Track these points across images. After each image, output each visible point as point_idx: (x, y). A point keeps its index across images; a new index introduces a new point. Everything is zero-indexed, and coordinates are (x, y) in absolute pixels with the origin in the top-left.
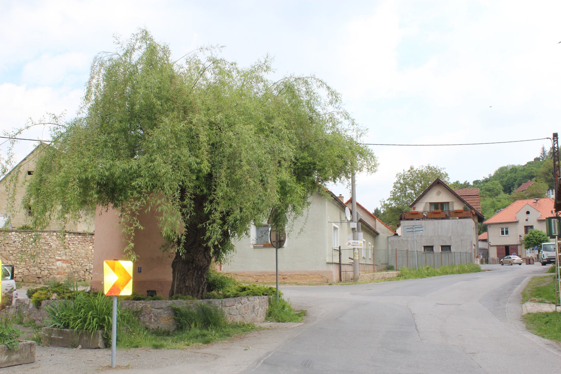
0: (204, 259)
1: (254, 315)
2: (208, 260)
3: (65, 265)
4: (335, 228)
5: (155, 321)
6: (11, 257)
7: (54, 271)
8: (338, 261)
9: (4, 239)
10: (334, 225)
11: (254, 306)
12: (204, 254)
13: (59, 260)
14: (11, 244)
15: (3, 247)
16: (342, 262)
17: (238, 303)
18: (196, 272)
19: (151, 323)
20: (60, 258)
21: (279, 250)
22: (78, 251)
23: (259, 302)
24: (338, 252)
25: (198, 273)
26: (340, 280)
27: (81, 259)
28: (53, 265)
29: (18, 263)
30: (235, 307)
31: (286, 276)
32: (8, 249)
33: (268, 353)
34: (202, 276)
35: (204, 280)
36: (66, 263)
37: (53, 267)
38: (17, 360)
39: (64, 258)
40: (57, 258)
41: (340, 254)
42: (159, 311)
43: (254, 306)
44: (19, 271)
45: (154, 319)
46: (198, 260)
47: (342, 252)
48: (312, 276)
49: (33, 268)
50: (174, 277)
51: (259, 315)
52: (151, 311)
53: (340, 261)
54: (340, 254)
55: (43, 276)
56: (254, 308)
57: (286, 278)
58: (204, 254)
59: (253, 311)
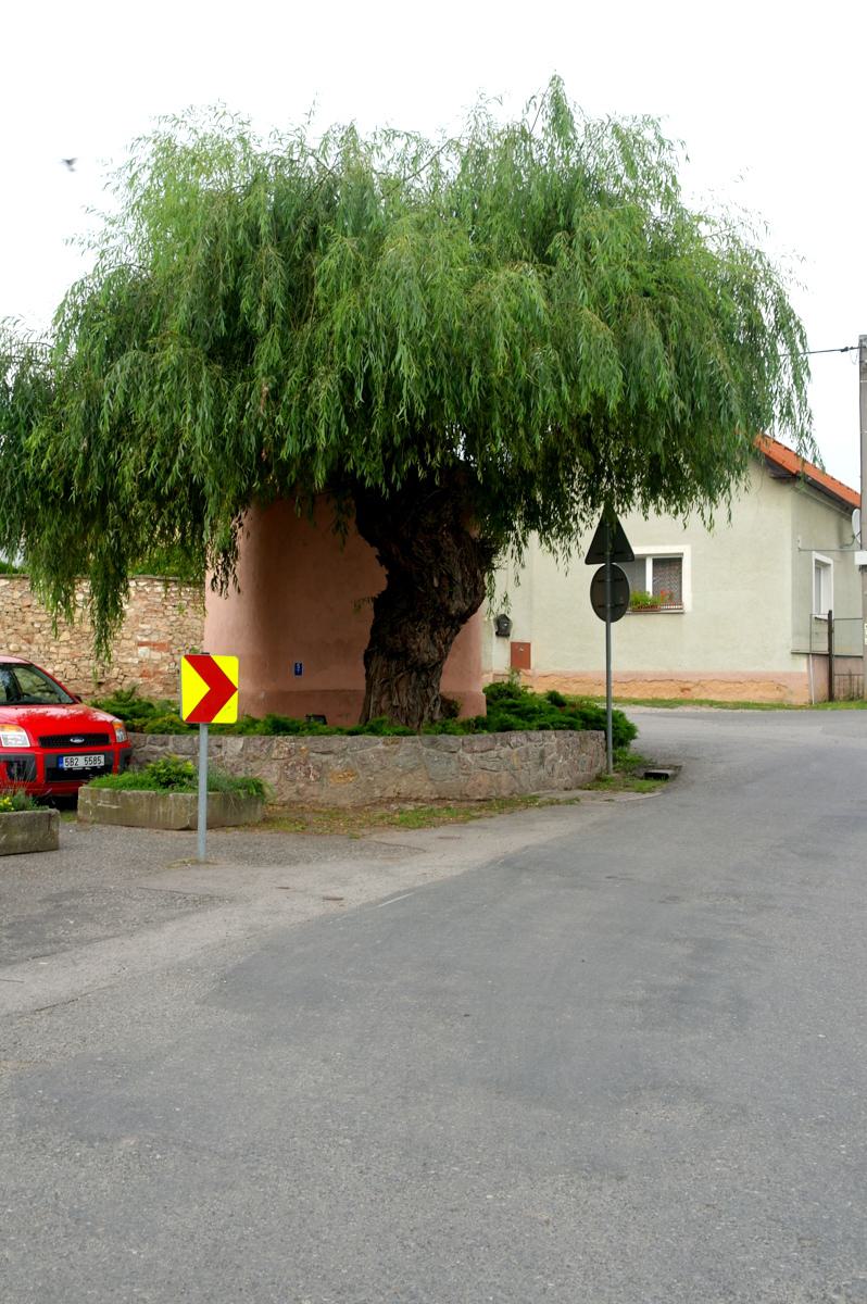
0: (432, 648)
1: (542, 772)
2: (440, 650)
3: (157, 656)
4: (820, 566)
5: (318, 780)
6: (37, 636)
7: (133, 670)
8: (824, 648)
9: (21, 597)
10: (817, 556)
11: (543, 751)
12: (432, 637)
13: (141, 644)
14: (36, 607)
15: (19, 615)
16: (836, 651)
17: (502, 745)
18: (414, 674)
19: (308, 783)
20: (145, 640)
21: (613, 625)
22: (187, 622)
23: (559, 744)
24: (825, 628)
25: (418, 678)
26: (831, 697)
27: (192, 642)
28: (131, 655)
29: (52, 649)
30: (493, 753)
31: (688, 685)
32: (30, 619)
33: (527, 847)
34: (428, 685)
35: (434, 694)
36: (159, 650)
37: (130, 660)
38: (24, 843)
39: (154, 638)
40: (139, 638)
41: (831, 632)
42: (325, 758)
43: (543, 751)
44: (57, 668)
45: (315, 776)
46: (419, 649)
47: (836, 625)
48: (755, 686)
49: (85, 663)
50: (809, 668)
51: (557, 772)
52: (309, 757)
53: (830, 649)
54: (831, 632)
55: (109, 681)
56: (542, 756)
57: (689, 689)
58: (432, 637)
59: (542, 763)
